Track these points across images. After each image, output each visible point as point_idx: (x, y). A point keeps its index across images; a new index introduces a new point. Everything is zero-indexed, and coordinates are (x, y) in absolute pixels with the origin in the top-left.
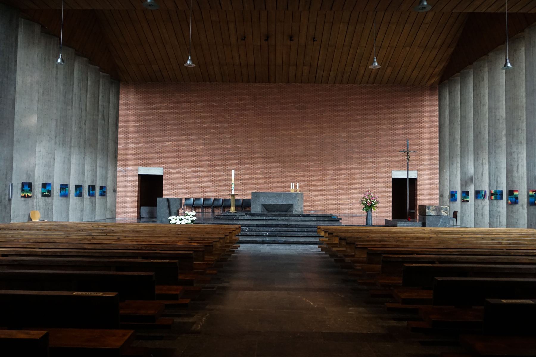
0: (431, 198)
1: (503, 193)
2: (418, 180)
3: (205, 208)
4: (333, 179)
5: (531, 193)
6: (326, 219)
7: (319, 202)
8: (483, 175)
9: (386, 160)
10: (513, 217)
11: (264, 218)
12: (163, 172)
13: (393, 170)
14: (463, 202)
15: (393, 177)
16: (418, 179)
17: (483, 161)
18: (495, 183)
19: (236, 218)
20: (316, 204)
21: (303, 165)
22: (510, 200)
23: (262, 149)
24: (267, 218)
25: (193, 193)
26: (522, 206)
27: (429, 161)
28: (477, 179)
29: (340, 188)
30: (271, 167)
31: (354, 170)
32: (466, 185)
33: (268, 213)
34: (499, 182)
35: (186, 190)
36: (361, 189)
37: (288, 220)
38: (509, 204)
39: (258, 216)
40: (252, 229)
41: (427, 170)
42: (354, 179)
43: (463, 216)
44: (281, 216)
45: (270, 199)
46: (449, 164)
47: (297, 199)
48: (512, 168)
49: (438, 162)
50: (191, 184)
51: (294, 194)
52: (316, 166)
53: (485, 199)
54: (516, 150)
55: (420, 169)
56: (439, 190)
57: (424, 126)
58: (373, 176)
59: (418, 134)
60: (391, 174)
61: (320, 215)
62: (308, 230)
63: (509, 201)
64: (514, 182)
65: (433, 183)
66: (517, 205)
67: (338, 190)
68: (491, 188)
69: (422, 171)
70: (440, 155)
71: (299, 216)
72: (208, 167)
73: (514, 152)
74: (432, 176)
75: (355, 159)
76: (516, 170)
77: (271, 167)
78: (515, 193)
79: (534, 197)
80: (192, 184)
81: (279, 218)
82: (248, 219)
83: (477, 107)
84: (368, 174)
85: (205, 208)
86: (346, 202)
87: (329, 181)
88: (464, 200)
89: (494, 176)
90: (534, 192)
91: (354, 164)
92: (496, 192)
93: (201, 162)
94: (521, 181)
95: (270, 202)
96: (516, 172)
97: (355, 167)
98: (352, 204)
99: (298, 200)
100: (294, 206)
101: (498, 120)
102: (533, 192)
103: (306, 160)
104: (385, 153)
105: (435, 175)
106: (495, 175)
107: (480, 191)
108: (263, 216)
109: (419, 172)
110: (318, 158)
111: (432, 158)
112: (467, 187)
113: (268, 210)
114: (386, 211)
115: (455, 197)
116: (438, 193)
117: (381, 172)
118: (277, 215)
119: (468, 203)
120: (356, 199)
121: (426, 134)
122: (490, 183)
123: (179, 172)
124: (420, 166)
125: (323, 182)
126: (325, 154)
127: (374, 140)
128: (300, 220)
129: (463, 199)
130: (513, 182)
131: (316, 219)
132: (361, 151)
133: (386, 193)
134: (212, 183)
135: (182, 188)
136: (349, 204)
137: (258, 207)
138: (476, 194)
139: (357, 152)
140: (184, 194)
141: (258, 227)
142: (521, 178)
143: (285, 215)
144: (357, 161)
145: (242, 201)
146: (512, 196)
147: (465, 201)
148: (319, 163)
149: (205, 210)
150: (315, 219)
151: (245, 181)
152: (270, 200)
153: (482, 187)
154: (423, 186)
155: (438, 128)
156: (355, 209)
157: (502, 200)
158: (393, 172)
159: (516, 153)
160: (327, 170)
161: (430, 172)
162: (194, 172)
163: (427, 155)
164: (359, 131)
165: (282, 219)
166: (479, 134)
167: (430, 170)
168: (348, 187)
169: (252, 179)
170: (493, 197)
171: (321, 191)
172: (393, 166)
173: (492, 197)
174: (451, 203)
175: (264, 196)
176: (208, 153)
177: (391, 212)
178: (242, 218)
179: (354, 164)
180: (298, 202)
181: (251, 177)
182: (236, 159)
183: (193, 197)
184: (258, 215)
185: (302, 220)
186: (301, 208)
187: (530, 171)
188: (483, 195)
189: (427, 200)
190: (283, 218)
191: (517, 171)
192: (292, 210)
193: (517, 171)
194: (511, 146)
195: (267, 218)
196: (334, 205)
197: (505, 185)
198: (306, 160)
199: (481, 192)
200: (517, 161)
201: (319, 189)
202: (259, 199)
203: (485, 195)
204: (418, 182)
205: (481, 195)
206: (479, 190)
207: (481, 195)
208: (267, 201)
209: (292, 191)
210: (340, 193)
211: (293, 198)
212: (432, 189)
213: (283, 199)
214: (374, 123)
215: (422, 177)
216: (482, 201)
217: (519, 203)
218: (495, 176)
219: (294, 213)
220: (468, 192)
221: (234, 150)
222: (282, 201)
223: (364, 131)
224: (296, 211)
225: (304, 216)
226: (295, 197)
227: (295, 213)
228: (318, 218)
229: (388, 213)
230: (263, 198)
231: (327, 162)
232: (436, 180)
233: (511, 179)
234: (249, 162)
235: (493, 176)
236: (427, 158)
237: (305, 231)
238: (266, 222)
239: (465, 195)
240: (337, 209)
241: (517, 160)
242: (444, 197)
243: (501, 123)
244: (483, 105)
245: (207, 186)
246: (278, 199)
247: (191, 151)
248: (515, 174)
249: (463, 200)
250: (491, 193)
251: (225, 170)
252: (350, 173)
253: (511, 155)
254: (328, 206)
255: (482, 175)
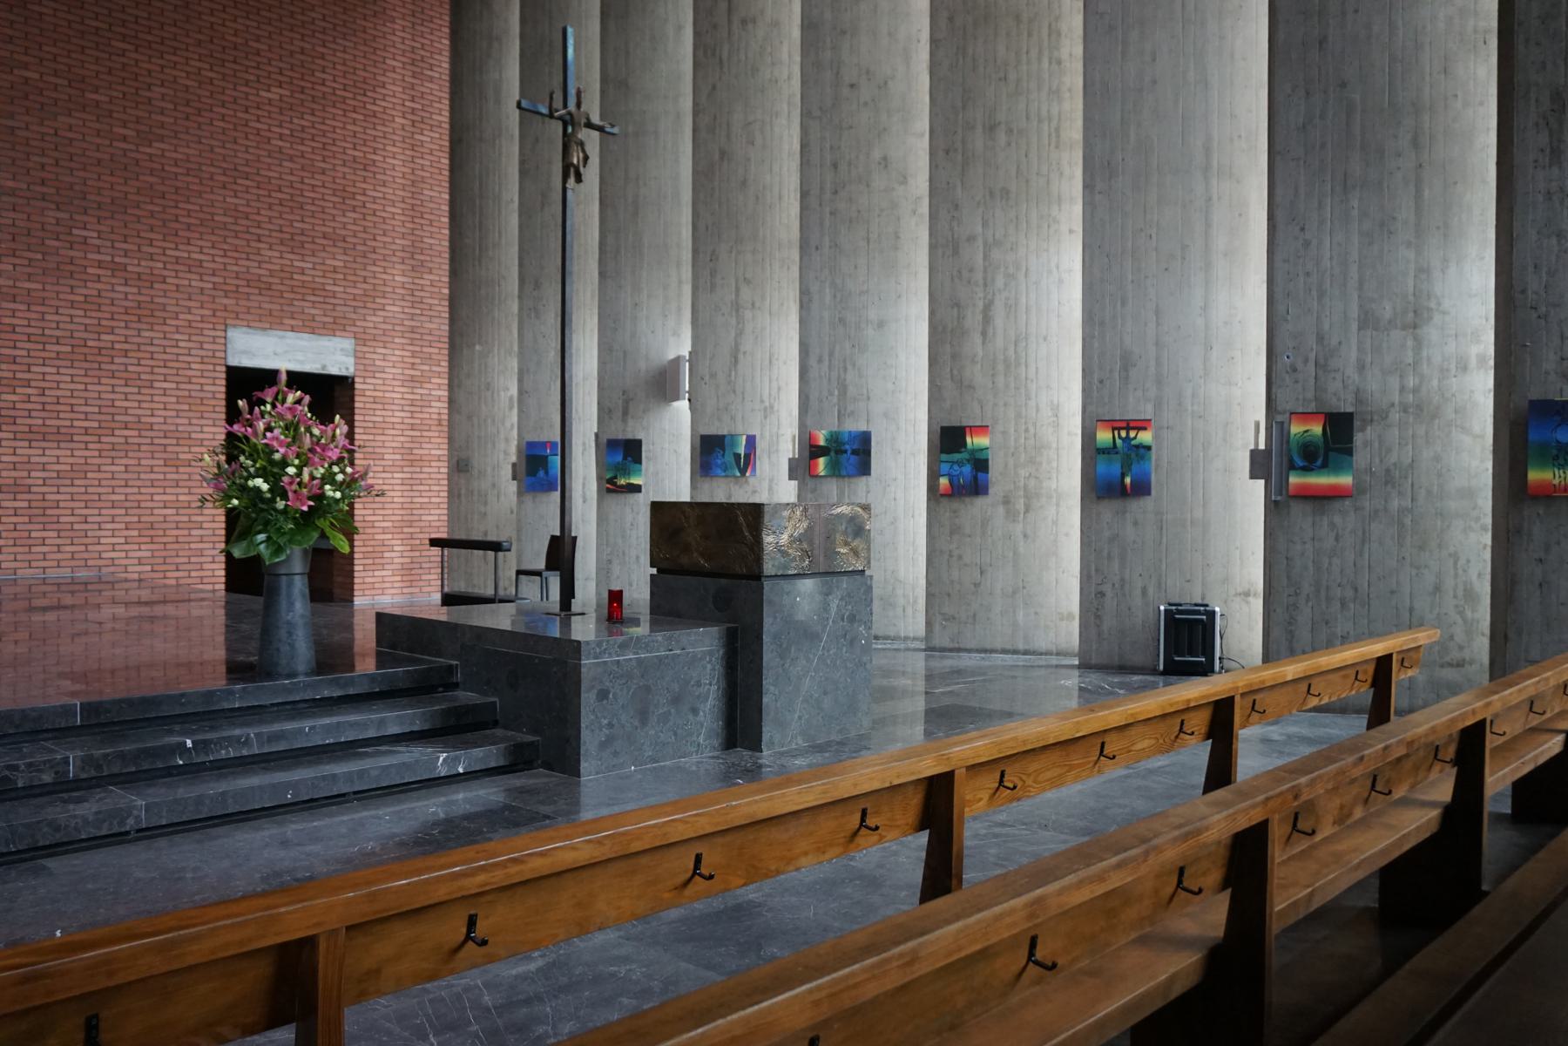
0: (415, 476)
1: (873, 444)
2: (357, 386)
5: (1104, 437)
8: (741, 356)
10: (960, 557)
13: (234, 326)
14: (609, 491)
15: (234, 361)
16: (357, 380)
17: (738, 290)
18: (831, 394)
22: (950, 476)
26: (1006, 501)
27: (407, 298)
28: (707, 378)
32: (625, 413)
34: (851, 390)
38: (942, 495)
41: (397, 340)
43: (610, 561)
46: (521, 309)
48: (961, 318)
49: (447, 303)
53: (748, 474)
54: (979, 229)
55: (368, 331)
56: (451, 440)
57: (385, 117)
58: (117, 346)
59: (356, 153)
63: (944, 481)
64: (971, 387)
65: (425, 403)
66: (980, 501)
68: (809, 422)
69: (374, 344)
70: (455, 273)
73: (971, 239)
74: (422, 371)
76: (980, 328)
78: (975, 441)
79: (1118, 456)
83: (715, 27)
84: (85, 335)
88: (614, 484)
89: (826, 358)
90: (1119, 429)
92: (835, 439)
94: (1000, 380)
96: (978, 339)
101: (852, 86)
102: (1114, 429)
104: (189, 227)
105: (434, 368)
106: (831, 354)
107: (724, 436)
109: (365, 349)
111: (421, 282)
112: (631, 422)
114: (193, 546)
115: (547, 473)
116: (446, 452)
117: (166, 328)
119: (636, 496)
121: (395, 162)
122: (807, 397)
124: (368, 318)
127: (125, 139)
129: (608, 476)
130: (964, 386)
132: (38, 188)
138: (702, 453)
142: (1001, 367)
146: (956, 456)
147: (622, 486)
153: (733, 418)
154: (381, 419)
155: (447, 144)
157: (864, 478)
158: (230, 334)
159: (980, 242)
161: (411, 348)
163: (397, 266)
164: (26, 66)
166: (722, 159)
167: (412, 339)
170: (822, 461)
172: (233, 302)
173: (816, 465)
174: (528, 498)
187: (1102, 324)
188: (737, 456)
189: (396, 488)
191: (984, 334)
193: (984, 334)
194: (956, 207)
197: (1485, 344)
199: (727, 440)
200: (985, 285)
203: (747, 456)
204: (357, 399)
205: (729, 458)
206: (720, 433)
207: (729, 458)
212: (418, 434)
214: (124, 38)
215: (377, 375)
216: (732, 485)
217: (991, 491)
218: (830, 361)
220: (640, 442)
223: (56, 74)
232: (438, 390)
233: (955, 372)
235: (820, 361)
236: (397, 278)
239: (619, 458)
241: (985, 279)
242: (475, 472)
243: (866, 104)
244: (744, 22)
248: (974, 344)
249: (611, 481)
250: (811, 446)
253: (956, 252)
255: (736, 361)
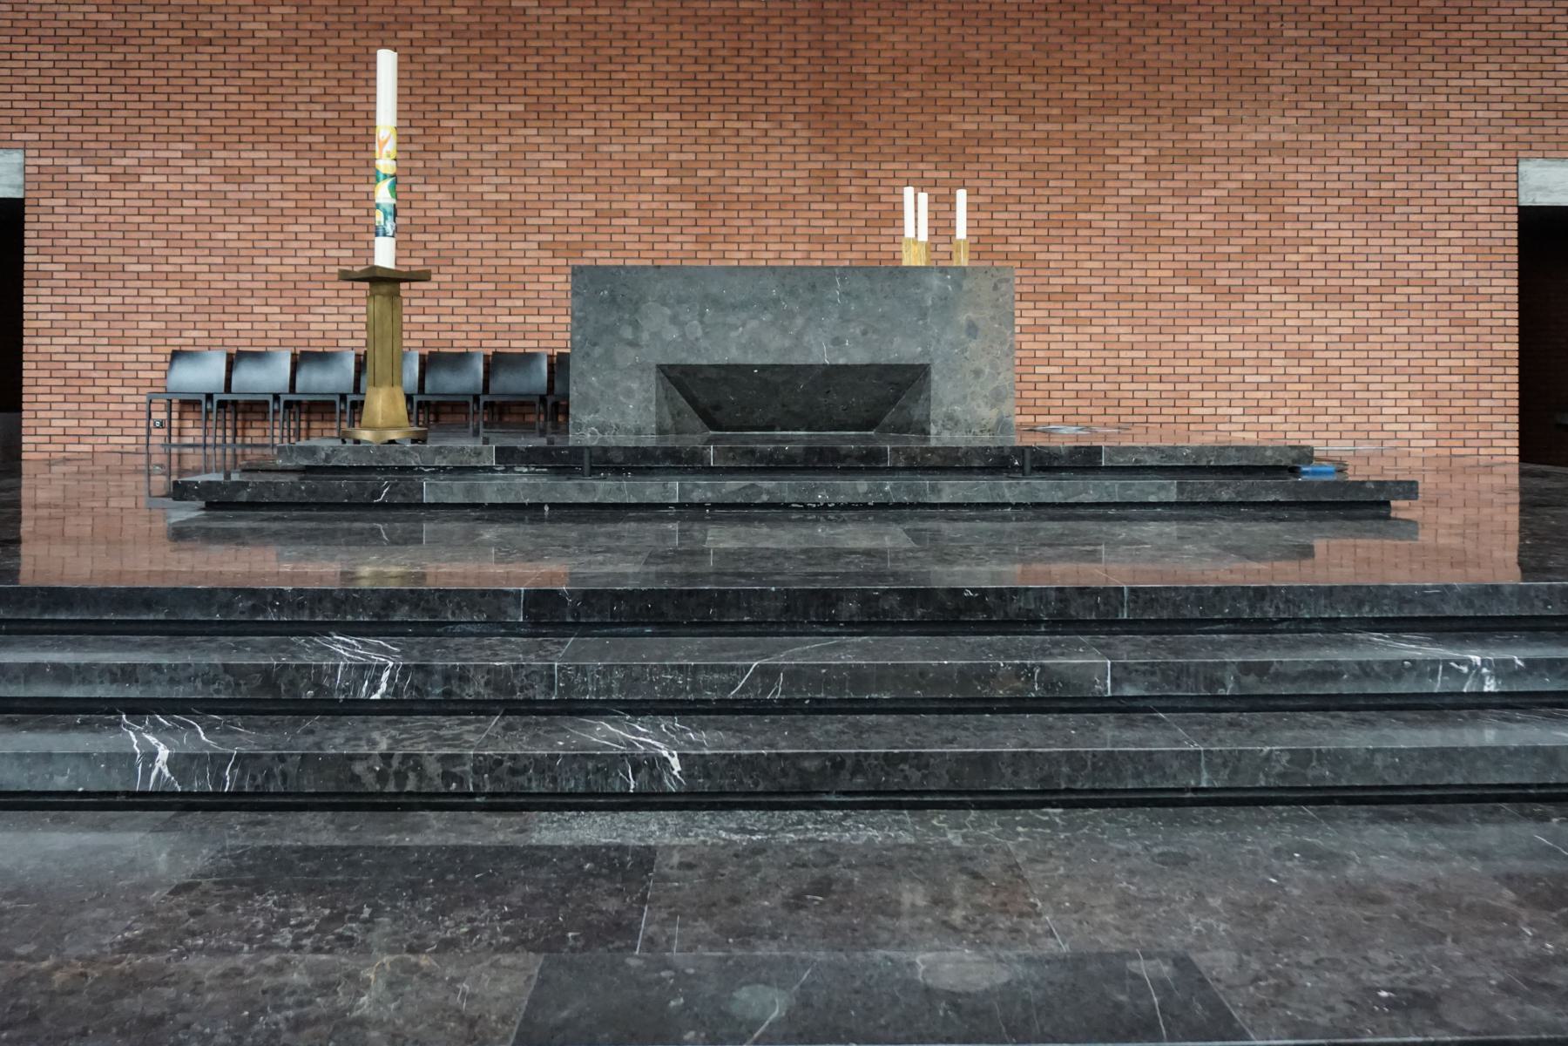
3: (309, 412)
4: (1146, 217)
6: (1268, 489)
7: (1059, 370)
9: (1481, 96)
11: (672, 489)
12: (19, 179)
13: (1528, 158)
15: (1526, 201)
19: (398, 499)
20: (1035, 378)
21: (950, 127)
23: (677, 28)
24: (703, 490)
25: (224, 317)
29: (1189, 275)
30: (739, 140)
31: (1275, 160)
33: (710, 441)
35: (176, 301)
36: (1322, 282)
37: (900, 505)
39: (618, 471)
40: (447, 676)
42: (1278, 217)
44: (834, 470)
45: (731, 319)
47: (963, 318)
50: (210, 260)
51: (935, 281)
52: (1034, 135)
60: (1514, 185)
61: (1200, 450)
62: (1262, 669)
67: (1178, 290)
71: (1001, 463)
72: (323, 147)
75: (1283, 89)
77: (739, 140)
80: (220, 260)
81: (813, 491)
82: (510, 499)
85: (309, 412)
86: (1231, 362)
87: (1119, 233)
91: (1275, 120)
93: (278, 114)
95: (728, 350)
97: (1284, 137)
98: (1267, 379)
99: (972, 329)
100: (935, 376)
103: (966, 94)
108: (668, 471)
110: (1046, 79)
113: (718, 415)
114: (1481, 418)
118: (790, 457)
120: (1295, 346)
123: (125, 178)
125: (1079, 240)
126: (1091, 56)
128: (1018, 506)
131: (1173, 497)
133: (1481, 306)
134: (350, 253)
135: (148, 284)
136: (1248, 379)
137: (629, 393)
139: (1295, 42)
140: (162, 325)
141: (561, 629)
143: (870, 463)
144: (1294, 97)
145: (551, 365)
148: (1056, 111)
149: (308, 428)
150: (1170, 491)
151: (568, 238)
152: (733, 334)
156: (1287, 411)
158: (1523, 167)
160: (1102, 160)
162: (232, 176)
165: (842, 499)
168: (1238, 265)
169: (615, 221)
171: (1069, 295)
175: (680, 301)
176: (325, 50)
177: (1513, 425)
178: (456, 491)
179: (1275, 120)
180: (973, 345)
181: (606, 206)
182: (510, 92)
183: (227, 342)
184: (619, 458)
185: (1038, 505)
186: (997, 398)
190: (860, 487)
192: (917, 413)
195: (703, 490)
196: (1151, 386)
198: (966, 94)
201: (1052, 281)
202: (636, 326)
208: (704, 343)
209: (912, 257)
210: (1193, 306)
211: (924, 316)
213: (845, 319)
219: (933, 443)
221: (493, 34)
222: (837, 342)
224: (952, 421)
225: (1044, 463)
226: (946, 304)
227: (946, 435)
228: (1194, 482)
229: (1493, 435)
230: (668, 311)
231: (1106, 105)
234: (593, 108)
237: (1229, 689)
238: (232, 965)
240: (1171, 411)
245: (320, 269)
246: (799, 321)
247: (210, 42)
251: (437, 164)
252: (1252, 177)
254: (1117, 394)
